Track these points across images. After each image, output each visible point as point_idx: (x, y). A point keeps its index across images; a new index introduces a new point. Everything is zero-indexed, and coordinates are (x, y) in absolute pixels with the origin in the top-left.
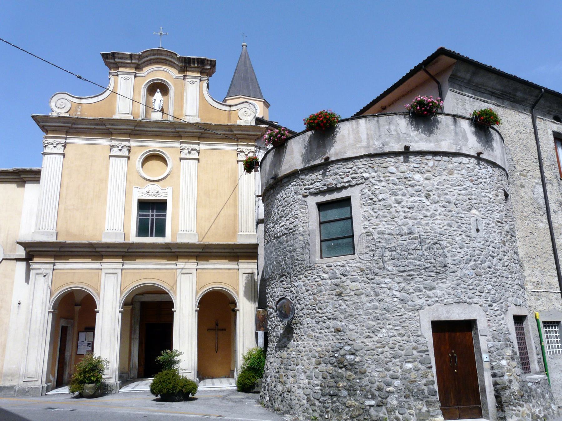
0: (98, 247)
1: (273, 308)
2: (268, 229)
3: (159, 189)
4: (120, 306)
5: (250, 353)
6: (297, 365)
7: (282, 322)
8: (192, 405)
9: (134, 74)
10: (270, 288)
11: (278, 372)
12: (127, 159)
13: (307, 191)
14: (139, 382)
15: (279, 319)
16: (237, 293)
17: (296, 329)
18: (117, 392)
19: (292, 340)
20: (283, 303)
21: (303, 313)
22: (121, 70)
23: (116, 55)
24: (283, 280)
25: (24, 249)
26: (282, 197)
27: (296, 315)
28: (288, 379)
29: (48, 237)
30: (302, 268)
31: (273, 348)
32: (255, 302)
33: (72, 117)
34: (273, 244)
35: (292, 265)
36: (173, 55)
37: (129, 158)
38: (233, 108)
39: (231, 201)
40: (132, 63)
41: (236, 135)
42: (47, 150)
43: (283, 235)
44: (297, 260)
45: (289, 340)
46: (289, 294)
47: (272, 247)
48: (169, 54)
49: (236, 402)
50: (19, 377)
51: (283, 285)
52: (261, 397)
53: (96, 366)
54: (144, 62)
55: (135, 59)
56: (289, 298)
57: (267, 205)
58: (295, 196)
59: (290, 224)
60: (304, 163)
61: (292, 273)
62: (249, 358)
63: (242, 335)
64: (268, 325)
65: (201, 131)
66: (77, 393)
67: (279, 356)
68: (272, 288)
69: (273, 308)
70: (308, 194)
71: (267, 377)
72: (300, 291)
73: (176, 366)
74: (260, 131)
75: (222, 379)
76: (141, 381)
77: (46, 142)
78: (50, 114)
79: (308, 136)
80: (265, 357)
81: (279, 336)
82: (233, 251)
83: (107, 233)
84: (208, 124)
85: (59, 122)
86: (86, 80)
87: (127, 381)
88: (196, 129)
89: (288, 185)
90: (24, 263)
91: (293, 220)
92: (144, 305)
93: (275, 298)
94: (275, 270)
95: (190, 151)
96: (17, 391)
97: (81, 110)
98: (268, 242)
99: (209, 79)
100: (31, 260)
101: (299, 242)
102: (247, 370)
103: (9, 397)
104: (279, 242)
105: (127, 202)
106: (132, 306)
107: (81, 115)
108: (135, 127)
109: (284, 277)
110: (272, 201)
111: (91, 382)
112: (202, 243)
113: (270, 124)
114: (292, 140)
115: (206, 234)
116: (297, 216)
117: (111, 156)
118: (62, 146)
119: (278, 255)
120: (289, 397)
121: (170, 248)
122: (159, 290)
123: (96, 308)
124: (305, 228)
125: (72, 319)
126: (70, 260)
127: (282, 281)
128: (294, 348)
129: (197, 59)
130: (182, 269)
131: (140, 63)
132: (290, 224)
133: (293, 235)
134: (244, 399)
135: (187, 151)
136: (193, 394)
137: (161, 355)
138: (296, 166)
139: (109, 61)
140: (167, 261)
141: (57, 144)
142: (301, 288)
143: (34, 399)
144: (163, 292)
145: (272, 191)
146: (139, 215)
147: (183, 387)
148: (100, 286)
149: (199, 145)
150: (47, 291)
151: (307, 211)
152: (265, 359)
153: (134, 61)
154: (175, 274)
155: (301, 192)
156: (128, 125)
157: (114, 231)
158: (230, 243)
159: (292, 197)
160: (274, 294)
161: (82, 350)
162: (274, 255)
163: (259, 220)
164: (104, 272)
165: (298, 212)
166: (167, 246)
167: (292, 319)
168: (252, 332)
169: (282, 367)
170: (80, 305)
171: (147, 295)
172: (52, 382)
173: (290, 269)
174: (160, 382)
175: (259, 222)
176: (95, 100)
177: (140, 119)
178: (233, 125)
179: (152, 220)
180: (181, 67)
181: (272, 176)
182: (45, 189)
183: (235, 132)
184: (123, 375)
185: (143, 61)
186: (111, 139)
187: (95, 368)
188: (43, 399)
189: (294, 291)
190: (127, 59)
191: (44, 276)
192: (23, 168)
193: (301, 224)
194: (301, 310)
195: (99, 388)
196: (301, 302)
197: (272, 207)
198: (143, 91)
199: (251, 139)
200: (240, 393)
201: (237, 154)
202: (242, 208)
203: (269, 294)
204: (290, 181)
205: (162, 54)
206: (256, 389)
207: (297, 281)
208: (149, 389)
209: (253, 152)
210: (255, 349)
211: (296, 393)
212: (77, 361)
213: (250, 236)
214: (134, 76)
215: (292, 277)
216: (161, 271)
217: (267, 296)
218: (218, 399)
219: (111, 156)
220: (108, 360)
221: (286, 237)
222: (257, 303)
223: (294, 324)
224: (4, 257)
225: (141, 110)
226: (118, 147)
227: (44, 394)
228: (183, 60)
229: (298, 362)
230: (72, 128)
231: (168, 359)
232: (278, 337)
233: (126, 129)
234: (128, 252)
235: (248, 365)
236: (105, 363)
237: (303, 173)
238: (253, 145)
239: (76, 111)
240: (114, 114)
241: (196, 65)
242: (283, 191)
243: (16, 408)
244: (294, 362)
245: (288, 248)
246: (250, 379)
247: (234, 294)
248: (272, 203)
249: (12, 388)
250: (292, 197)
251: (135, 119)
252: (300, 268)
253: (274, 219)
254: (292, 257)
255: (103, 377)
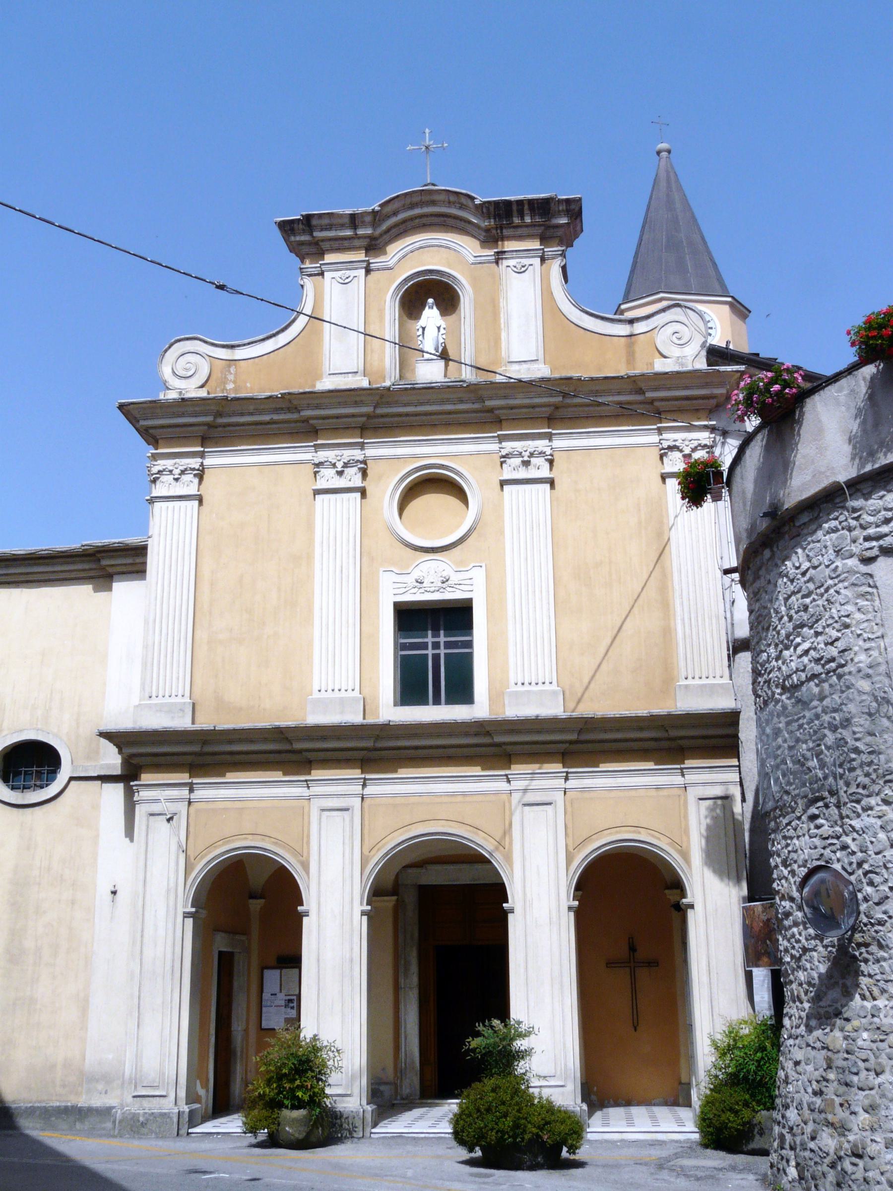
0: (299, 740)
1: (792, 899)
2: (762, 665)
3: (448, 572)
4: (362, 899)
5: (732, 1033)
6: (877, 1074)
7: (822, 941)
8: (571, 1183)
9: (364, 265)
10: (779, 837)
11: (818, 1093)
12: (358, 495)
13: (874, 543)
14: (424, 1110)
15: (811, 931)
16: (686, 856)
17: (866, 961)
18: (367, 1134)
19: (857, 997)
20: (823, 881)
21: (885, 913)
22: (329, 258)
23: (314, 222)
24: (816, 812)
25: (116, 750)
26: (797, 568)
27: (865, 920)
28: (853, 1117)
29: (173, 718)
30: (874, 776)
31: (800, 1017)
32: (738, 880)
33: (214, 398)
34: (779, 707)
35: (841, 766)
36: (463, 200)
37: (363, 492)
38: (640, 327)
39: (651, 592)
40: (356, 237)
41: (652, 402)
42: (159, 490)
43: (809, 679)
44: (856, 750)
45: (848, 995)
46: (838, 854)
47: (778, 716)
48: (452, 198)
49: (698, 1179)
50: (123, 1084)
51: (818, 827)
52: (772, 1166)
53: (308, 1061)
54: (388, 230)
55: (364, 225)
56: (837, 866)
57: (756, 594)
58: (839, 563)
59: (826, 644)
60: (857, 461)
61: (842, 793)
62: (730, 1049)
63: (705, 979)
64: (781, 948)
65: (552, 400)
66: (263, 1135)
67: (818, 1045)
68: (785, 838)
69: (792, 899)
70: (875, 552)
71: (786, 1107)
72: (870, 846)
73: (521, 1067)
74: (721, 385)
75: (656, 1109)
76: (430, 1105)
77: (155, 470)
78: (161, 397)
79: (864, 379)
80: (777, 1045)
81: (817, 981)
82: (666, 735)
83: (319, 700)
84: (570, 379)
85: (182, 415)
86: (238, 292)
87: (394, 1105)
88: (540, 396)
89: (815, 531)
90: (120, 787)
91: (835, 634)
92: (426, 893)
93: (795, 866)
94: (791, 784)
95: (526, 458)
96: (120, 1122)
97: (235, 377)
98: (766, 703)
99: (567, 253)
100: (136, 780)
101: (858, 699)
102: (726, 1084)
103: (101, 1136)
104: (799, 701)
105: (365, 613)
106: (394, 898)
107: (235, 390)
108: (375, 407)
109: (820, 804)
110: (769, 582)
111: (298, 1105)
112: (575, 714)
113: (754, 361)
114: (816, 397)
115: (587, 688)
116: (847, 620)
117: (317, 492)
118: (195, 475)
119: (798, 740)
120: (859, 1175)
121: (488, 734)
122: (472, 853)
123: (302, 904)
124: (875, 653)
125: (243, 933)
126: (228, 774)
127: (813, 818)
128: (864, 1021)
129: (531, 202)
130: (525, 790)
131: (378, 232)
132: (826, 644)
133: (840, 677)
134: (721, 1169)
135: (518, 461)
136: (573, 1149)
137: (478, 1034)
138: (834, 474)
139: (298, 238)
140: (483, 769)
141: (183, 472)
142: (875, 835)
143: (160, 1143)
144: (479, 859)
145: (767, 553)
146: (399, 647)
147: (541, 1128)
148: (308, 843)
149: (550, 440)
150: (178, 858)
151: (877, 603)
152: (779, 1051)
153: (361, 232)
154: (507, 804)
155: (855, 549)
156: (356, 404)
157: (337, 694)
158: (656, 711)
159: (827, 566)
160: (794, 856)
161: (274, 1018)
162: (785, 741)
163: (735, 641)
164: (316, 804)
165: (850, 608)
166: (481, 728)
167: (854, 929)
168: (735, 970)
169: (832, 1076)
170: (261, 898)
171: (438, 867)
172: (204, 1101)
173: (835, 778)
174: (478, 1110)
175: (738, 647)
176: (270, 345)
177: (387, 383)
178: (643, 375)
179: (436, 658)
180: (487, 230)
181: (765, 509)
182: (159, 591)
183: (649, 395)
184: (382, 1088)
185: (384, 227)
186: (315, 446)
187: (305, 1066)
188: (182, 1145)
189: (853, 847)
190: (342, 226)
191: (169, 820)
192: (106, 541)
193: (861, 643)
194: (877, 904)
195: (318, 1122)
196: (877, 879)
197: (771, 601)
198: (391, 308)
199: (697, 410)
200: (709, 1152)
201: (661, 457)
202: (686, 609)
203: (779, 856)
204: (817, 518)
205: (433, 203)
206: (756, 1144)
207: (859, 816)
208: (451, 1131)
209: (705, 446)
210: (746, 1022)
211: (882, 1161)
212: (261, 1046)
213: (712, 689)
214: (362, 272)
215: (845, 804)
216: (468, 799)
217: (772, 862)
218: (644, 1168)
219: (317, 492)
220: (338, 1045)
221: (817, 685)
222: (744, 885)
223: (859, 945)
224: (73, 771)
225: (389, 357)
226: (334, 465)
227: (183, 1131)
228: (492, 209)
229: (880, 1064)
230: (216, 427)
231: (495, 1045)
232: (813, 986)
233: (353, 416)
234: (376, 749)
235: (730, 1070)
236: (331, 1054)
237: (858, 490)
238: (706, 427)
239: (224, 381)
240: (319, 377)
241: (528, 220)
242: (800, 551)
243: (115, 1167)
244: (867, 1064)
245: (826, 718)
246: (736, 1112)
247: (674, 858)
248: (771, 587)
249: (106, 1112)
250: (827, 566)
251: (374, 386)
252: (867, 775)
253: (778, 633)
254: (841, 743)
255: (328, 1091)
